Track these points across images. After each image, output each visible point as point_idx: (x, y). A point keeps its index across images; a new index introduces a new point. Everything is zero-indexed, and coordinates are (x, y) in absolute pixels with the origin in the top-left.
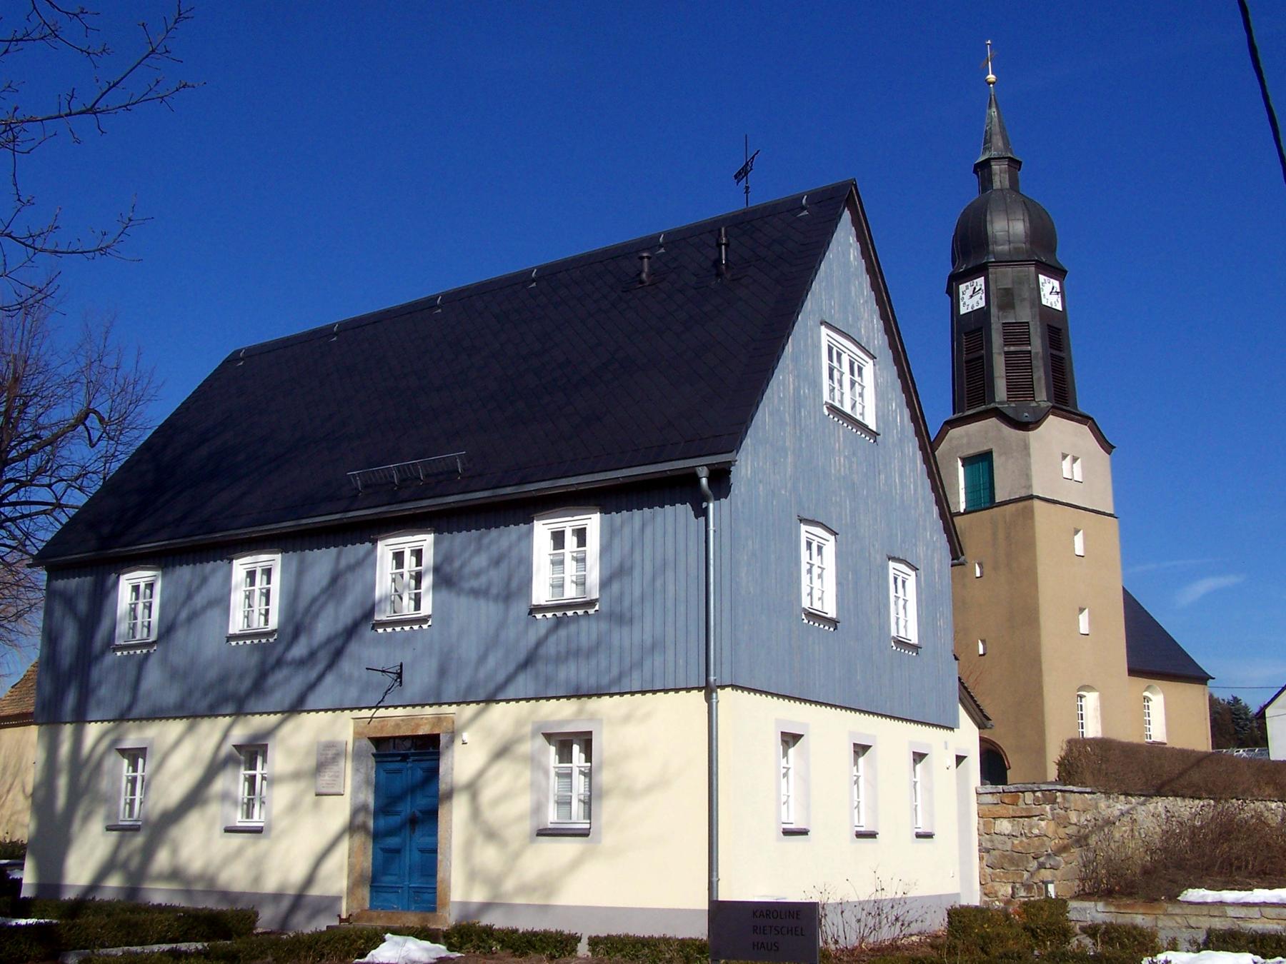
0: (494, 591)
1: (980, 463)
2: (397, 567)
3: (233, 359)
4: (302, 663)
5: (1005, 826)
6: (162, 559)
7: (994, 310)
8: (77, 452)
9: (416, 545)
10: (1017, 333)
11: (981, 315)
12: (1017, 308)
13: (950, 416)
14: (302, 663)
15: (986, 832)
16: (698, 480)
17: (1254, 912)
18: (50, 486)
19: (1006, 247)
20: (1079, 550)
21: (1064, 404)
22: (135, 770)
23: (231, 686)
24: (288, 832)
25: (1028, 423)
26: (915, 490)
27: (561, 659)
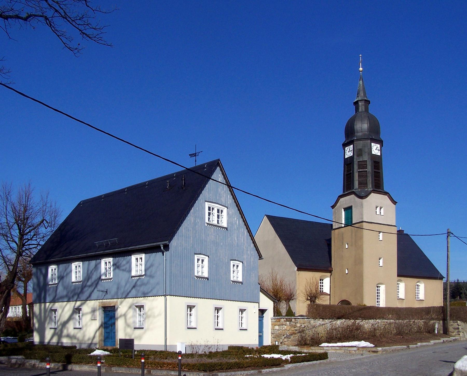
0: (127, 270)
1: (349, 210)
2: (106, 264)
3: (79, 204)
4: (90, 286)
5: (277, 327)
6: (57, 263)
7: (355, 157)
8: (42, 230)
9: (109, 261)
10: (362, 165)
11: (351, 158)
12: (363, 156)
13: (341, 193)
14: (90, 286)
15: (273, 329)
16: (161, 247)
17: (330, 348)
18: (36, 240)
19: (361, 134)
20: (381, 239)
21: (378, 188)
22: (140, 312)
23: (76, 291)
24: (86, 327)
25: (363, 197)
26: (244, 241)
27: (141, 286)
